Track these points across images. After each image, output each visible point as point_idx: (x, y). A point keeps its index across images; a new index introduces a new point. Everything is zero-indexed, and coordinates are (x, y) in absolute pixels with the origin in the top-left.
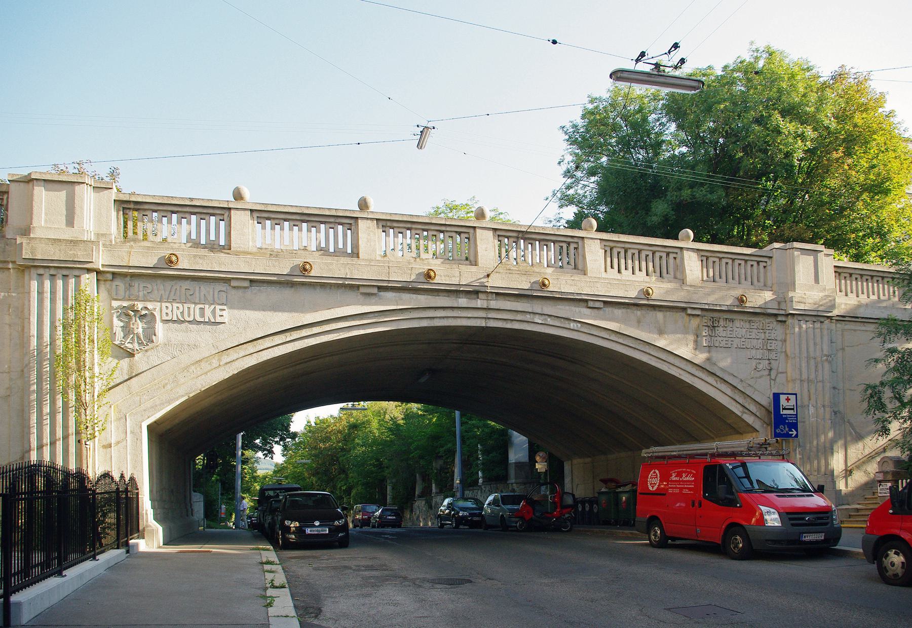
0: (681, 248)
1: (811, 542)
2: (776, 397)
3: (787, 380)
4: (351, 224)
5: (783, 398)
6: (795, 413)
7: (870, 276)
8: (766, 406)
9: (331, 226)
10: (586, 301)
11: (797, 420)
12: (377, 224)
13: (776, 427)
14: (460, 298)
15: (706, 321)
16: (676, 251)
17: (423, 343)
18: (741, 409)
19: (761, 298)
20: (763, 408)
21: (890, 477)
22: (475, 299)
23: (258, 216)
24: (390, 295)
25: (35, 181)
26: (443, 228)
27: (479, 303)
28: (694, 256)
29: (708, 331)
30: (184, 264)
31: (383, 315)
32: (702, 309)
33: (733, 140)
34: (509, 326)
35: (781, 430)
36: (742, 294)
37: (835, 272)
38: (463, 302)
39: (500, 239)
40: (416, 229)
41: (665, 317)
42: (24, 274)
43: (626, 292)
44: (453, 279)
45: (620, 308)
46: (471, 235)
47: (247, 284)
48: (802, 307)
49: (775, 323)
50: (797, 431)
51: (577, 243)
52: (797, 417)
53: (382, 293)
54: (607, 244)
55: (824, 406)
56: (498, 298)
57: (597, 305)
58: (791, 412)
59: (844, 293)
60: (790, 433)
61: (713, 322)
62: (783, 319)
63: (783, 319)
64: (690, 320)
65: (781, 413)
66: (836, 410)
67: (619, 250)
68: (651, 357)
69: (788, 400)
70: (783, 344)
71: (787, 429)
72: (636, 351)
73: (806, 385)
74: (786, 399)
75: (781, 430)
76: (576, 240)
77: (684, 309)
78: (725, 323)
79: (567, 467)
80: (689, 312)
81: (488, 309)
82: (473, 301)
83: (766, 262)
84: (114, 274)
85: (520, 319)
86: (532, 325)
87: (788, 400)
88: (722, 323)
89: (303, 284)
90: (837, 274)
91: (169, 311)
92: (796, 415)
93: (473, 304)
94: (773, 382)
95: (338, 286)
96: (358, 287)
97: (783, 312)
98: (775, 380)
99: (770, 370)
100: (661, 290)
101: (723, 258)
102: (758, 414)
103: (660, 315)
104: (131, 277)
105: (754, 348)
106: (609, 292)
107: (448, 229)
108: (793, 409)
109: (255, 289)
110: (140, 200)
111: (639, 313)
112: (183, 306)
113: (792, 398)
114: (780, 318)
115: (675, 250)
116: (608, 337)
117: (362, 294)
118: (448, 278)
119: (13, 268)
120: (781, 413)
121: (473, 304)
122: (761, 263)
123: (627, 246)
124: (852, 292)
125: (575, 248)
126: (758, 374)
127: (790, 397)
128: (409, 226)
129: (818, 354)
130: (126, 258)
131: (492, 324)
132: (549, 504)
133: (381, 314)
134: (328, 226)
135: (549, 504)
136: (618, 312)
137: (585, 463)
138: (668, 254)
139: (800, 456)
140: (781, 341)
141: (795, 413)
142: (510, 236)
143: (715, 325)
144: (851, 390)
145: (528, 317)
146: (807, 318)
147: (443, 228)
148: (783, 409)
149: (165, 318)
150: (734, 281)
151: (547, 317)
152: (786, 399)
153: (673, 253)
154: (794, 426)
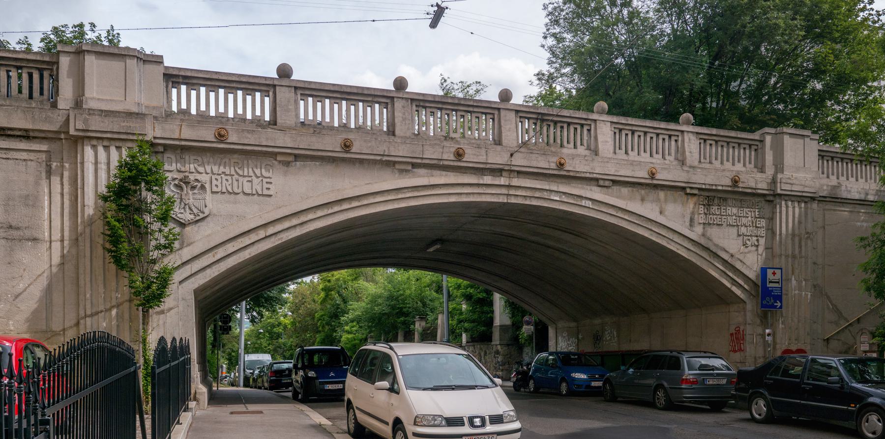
0: (682, 132)
1: (595, 387)
3: (773, 254)
4: (387, 103)
5: (770, 272)
6: (780, 286)
7: (850, 159)
8: (753, 279)
9: (369, 105)
11: (781, 293)
12: (411, 104)
13: (763, 298)
14: (485, 175)
15: (702, 200)
16: (589, 123)
17: (445, 217)
19: (756, 181)
20: (750, 281)
21: (875, 348)
22: (498, 176)
23: (302, 92)
24: (422, 171)
25: (86, 53)
26: (471, 109)
27: (503, 181)
28: (692, 137)
29: (704, 209)
30: (233, 138)
31: (416, 190)
32: (700, 189)
35: (767, 301)
36: (735, 175)
37: (819, 155)
38: (488, 179)
39: (521, 120)
40: (446, 109)
41: (666, 196)
42: (77, 145)
43: (633, 172)
44: (481, 157)
45: (626, 187)
46: (496, 116)
47: (410, 168)
48: (788, 187)
49: (764, 202)
50: (781, 302)
51: (590, 125)
52: (781, 290)
53: (415, 170)
54: (617, 126)
56: (520, 176)
57: (607, 183)
59: (825, 175)
60: (775, 304)
61: (708, 201)
63: (771, 198)
64: (688, 199)
65: (768, 286)
66: (815, 283)
67: (627, 132)
68: (652, 233)
70: (770, 222)
71: (772, 301)
72: (639, 227)
73: (790, 260)
74: (773, 273)
75: (767, 301)
76: (589, 122)
77: (684, 189)
78: (719, 201)
79: (551, 333)
80: (688, 191)
82: (497, 178)
83: (757, 145)
84: (165, 146)
85: (537, 196)
86: (549, 201)
87: (774, 274)
88: (716, 201)
89: (343, 160)
90: (820, 157)
91: (219, 183)
92: (781, 288)
95: (376, 163)
96: (395, 163)
100: (670, 173)
101: (719, 141)
104: (182, 150)
106: (618, 171)
107: (476, 110)
108: (778, 282)
110: (189, 74)
111: (643, 192)
112: (232, 178)
113: (778, 272)
114: (768, 198)
115: (676, 133)
116: (615, 214)
118: (475, 157)
119: (65, 139)
120: (768, 286)
122: (835, 159)
123: (634, 128)
124: (657, 153)
125: (588, 130)
126: (746, 250)
127: (776, 271)
128: (440, 106)
129: (803, 232)
130: (178, 131)
131: (513, 200)
133: (414, 189)
136: (625, 190)
137: (570, 327)
138: (670, 136)
139: (783, 326)
140: (768, 219)
141: (780, 286)
142: (531, 118)
143: (710, 203)
144: (829, 265)
145: (545, 195)
146: (793, 199)
147: (471, 109)
148: (770, 282)
149: (215, 189)
150: (728, 163)
151: (561, 194)
152: (773, 273)
153: (675, 135)
154: (779, 298)
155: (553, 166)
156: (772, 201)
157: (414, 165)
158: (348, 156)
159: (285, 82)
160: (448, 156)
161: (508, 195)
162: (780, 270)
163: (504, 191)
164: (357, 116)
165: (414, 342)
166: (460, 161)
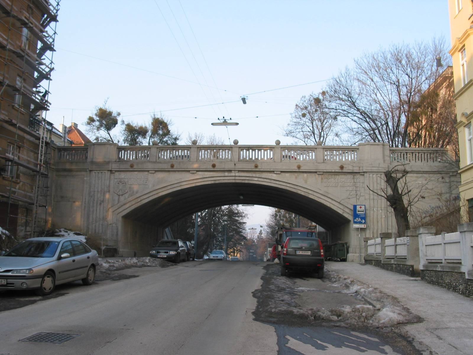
2: (355, 207)
5: (358, 208)
10: (274, 171)
18: (342, 211)
24: (200, 173)
33: (368, 87)
34: (243, 182)
38: (226, 174)
41: (307, 175)
47: (280, 173)
53: (198, 173)
55: (98, 191)
56: (239, 172)
57: (278, 173)
58: (362, 213)
62: (363, 174)
63: (363, 174)
65: (357, 213)
69: (361, 207)
77: (316, 172)
81: (235, 176)
87: (361, 207)
93: (230, 175)
94: (358, 200)
97: (362, 171)
98: (359, 199)
99: (357, 195)
102: (350, 213)
103: (305, 175)
105: (349, 186)
108: (363, 211)
109: (157, 173)
117: (318, 174)
121: (230, 175)
127: (361, 206)
132: (9, 205)
134: (211, 150)
135: (9, 205)
155: (253, 167)
156: (364, 175)
157: (197, 171)
158: (173, 170)
159: (278, 146)
160: (210, 167)
161: (235, 179)
162: (364, 206)
163: (233, 178)
164: (225, 155)
165: (17, 218)
166: (173, 168)
